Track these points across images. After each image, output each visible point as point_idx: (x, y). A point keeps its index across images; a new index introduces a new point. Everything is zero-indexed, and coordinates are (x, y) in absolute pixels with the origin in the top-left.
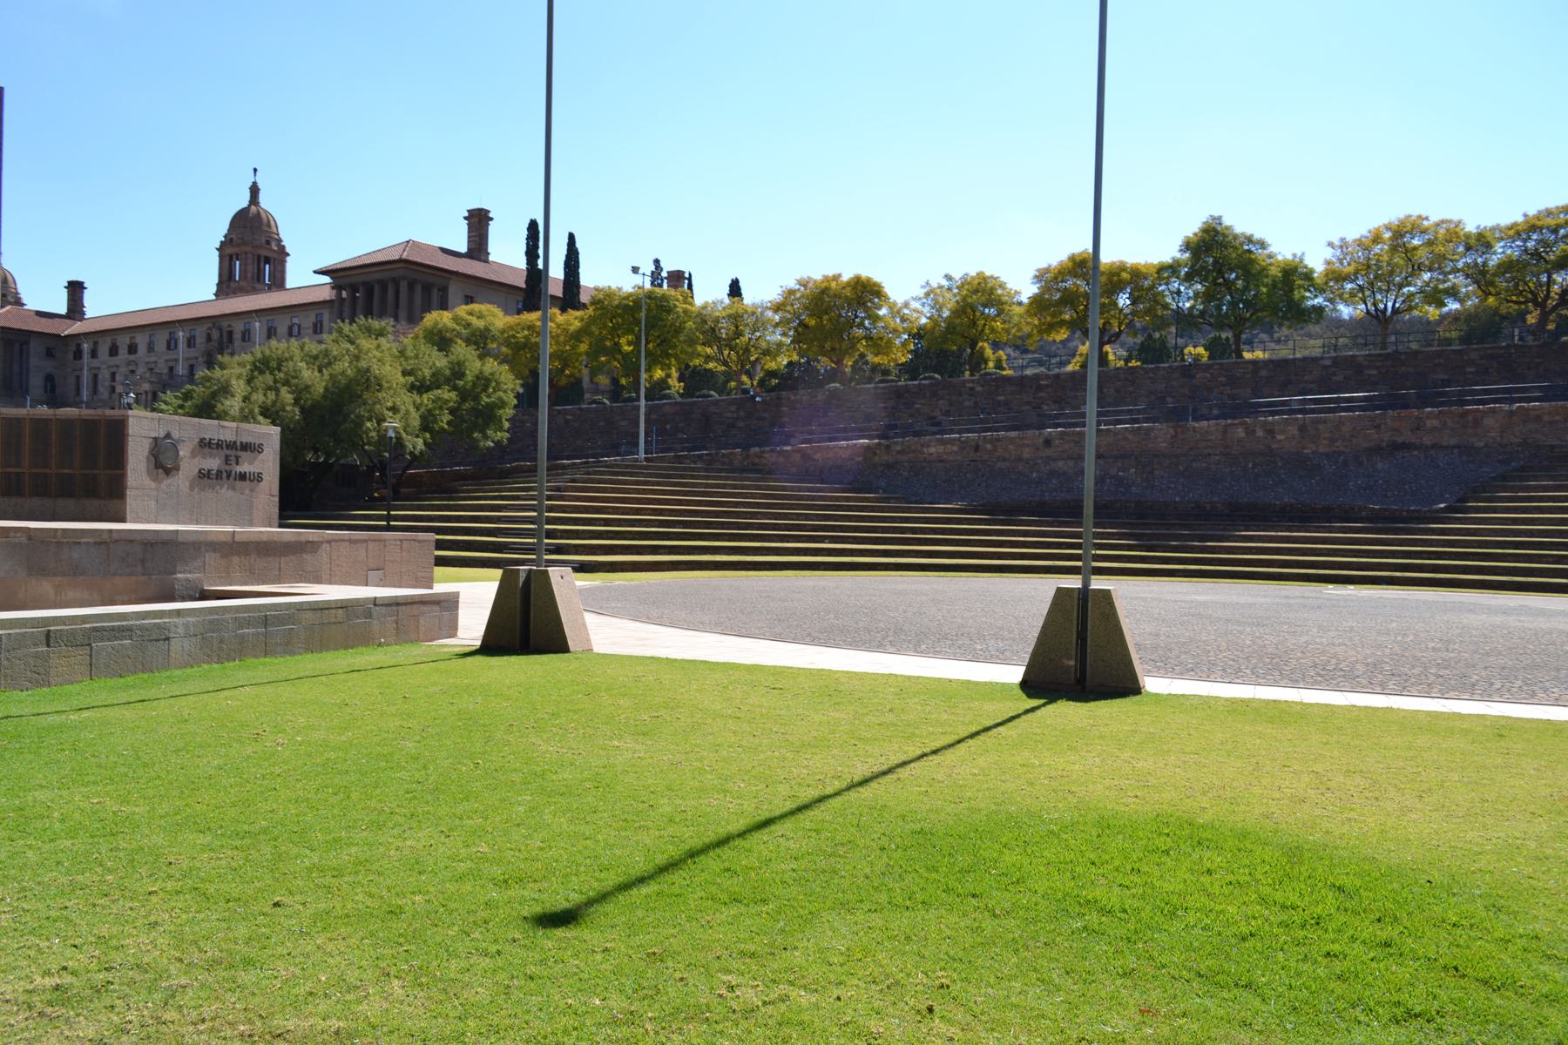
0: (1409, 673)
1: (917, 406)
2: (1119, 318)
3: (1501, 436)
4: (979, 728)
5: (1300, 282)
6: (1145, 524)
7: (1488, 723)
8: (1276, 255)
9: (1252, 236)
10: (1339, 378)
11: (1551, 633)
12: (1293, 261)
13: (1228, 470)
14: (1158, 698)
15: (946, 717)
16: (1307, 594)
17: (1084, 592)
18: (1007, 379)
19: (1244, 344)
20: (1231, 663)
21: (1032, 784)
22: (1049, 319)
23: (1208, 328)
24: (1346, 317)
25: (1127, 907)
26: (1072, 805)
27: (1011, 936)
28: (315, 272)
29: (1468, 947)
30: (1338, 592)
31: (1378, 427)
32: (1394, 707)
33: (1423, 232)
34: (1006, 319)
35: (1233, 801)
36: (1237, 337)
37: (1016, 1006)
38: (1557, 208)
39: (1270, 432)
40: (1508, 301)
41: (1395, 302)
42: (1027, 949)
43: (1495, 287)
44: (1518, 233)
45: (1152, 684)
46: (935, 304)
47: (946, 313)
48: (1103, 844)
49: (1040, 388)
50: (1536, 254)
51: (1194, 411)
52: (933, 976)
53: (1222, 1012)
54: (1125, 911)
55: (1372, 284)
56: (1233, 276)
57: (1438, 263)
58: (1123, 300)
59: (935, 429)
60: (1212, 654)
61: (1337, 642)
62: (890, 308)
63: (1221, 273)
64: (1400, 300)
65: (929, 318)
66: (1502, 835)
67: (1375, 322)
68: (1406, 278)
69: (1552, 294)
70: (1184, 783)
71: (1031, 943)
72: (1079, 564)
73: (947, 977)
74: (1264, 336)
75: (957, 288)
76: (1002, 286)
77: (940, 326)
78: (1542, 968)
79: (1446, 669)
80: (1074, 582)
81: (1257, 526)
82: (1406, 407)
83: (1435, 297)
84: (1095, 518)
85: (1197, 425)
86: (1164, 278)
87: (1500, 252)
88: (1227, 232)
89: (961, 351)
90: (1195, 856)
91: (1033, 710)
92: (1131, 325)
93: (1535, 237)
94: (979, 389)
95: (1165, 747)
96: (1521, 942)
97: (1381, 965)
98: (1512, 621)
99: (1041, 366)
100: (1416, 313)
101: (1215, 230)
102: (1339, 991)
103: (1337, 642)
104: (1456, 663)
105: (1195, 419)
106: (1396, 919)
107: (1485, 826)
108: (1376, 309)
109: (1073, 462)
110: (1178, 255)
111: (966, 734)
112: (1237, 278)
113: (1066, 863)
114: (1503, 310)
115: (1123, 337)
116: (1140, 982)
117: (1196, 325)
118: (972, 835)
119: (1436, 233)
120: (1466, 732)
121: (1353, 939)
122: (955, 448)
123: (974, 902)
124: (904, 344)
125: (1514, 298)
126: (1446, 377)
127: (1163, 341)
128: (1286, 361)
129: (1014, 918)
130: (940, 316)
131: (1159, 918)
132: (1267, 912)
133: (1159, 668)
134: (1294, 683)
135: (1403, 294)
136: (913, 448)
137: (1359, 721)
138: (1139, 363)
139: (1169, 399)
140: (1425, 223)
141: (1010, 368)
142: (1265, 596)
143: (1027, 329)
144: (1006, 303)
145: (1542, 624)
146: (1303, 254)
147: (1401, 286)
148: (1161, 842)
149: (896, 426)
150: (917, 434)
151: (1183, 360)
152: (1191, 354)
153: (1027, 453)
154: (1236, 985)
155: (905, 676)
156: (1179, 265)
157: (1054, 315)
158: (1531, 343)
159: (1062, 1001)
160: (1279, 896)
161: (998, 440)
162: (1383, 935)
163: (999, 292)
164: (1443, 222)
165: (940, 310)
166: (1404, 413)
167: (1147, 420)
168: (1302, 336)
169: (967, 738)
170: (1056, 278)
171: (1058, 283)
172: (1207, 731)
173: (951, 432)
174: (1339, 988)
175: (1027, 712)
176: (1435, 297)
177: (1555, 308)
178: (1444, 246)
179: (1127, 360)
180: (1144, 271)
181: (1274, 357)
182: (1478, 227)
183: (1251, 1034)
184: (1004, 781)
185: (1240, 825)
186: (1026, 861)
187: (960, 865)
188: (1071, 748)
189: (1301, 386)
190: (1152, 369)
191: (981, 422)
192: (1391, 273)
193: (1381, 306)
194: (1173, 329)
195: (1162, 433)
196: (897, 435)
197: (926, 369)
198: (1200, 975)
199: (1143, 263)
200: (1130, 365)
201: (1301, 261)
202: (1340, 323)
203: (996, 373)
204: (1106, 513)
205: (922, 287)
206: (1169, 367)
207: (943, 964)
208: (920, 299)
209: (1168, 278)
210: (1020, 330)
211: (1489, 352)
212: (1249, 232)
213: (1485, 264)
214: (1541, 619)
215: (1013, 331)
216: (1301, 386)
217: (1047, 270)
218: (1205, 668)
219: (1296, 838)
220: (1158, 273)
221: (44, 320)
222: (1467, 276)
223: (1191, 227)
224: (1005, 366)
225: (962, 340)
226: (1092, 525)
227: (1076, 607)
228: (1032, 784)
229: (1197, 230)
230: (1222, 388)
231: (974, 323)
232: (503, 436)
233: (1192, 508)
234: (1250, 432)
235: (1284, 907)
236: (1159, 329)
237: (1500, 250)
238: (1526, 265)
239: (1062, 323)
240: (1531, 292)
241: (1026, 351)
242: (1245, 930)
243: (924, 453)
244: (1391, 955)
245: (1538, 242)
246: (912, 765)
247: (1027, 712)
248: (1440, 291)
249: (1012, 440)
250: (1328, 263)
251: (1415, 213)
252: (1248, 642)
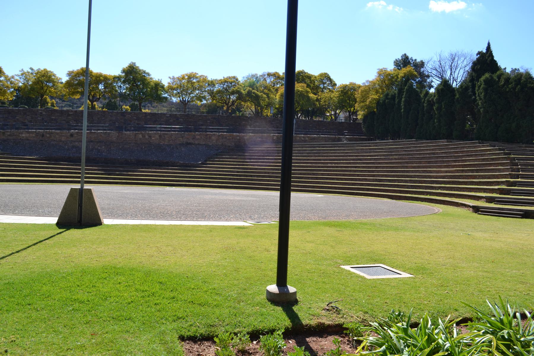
0: (188, 214)
2: (99, 93)
3: (216, 142)
4: (38, 241)
5: (160, 88)
6: (108, 166)
7: (208, 227)
8: (153, 78)
9: (145, 71)
10: (171, 121)
11: (227, 200)
12: (158, 81)
13: (136, 148)
14: (108, 226)
15: (24, 238)
16: (160, 190)
17: (81, 190)
18: (56, 110)
19: (142, 107)
20: (134, 213)
21: (57, 260)
22: (73, 90)
23: (131, 100)
24: (175, 102)
25: (89, 299)
26: (73, 266)
27: (43, 317)
29: (196, 295)
30: (170, 189)
31: (183, 137)
32: (183, 224)
33: (197, 78)
34: (56, 88)
35: (130, 259)
36: (140, 104)
37: (43, 342)
38: (232, 77)
39: (150, 137)
40: (219, 102)
41: (188, 99)
42: (49, 320)
43: (216, 98)
44: (222, 82)
45: (106, 221)
46: (26, 79)
47: (30, 83)
48: (83, 279)
49: (69, 115)
50: (226, 89)
51: (125, 128)
52: (9, 338)
53: (120, 329)
54: (89, 301)
55: (182, 92)
56: (139, 83)
57: (200, 88)
58: (101, 87)
59: (25, 127)
60: (128, 210)
61: (168, 205)
62: (5, 77)
63: (135, 82)
64: (190, 98)
65: (23, 84)
66: (208, 260)
67: (182, 104)
68: (192, 92)
69: (230, 102)
70: (114, 254)
71: (52, 318)
72: (85, 180)
73: (14, 338)
74: (149, 105)
75: (35, 73)
76: (54, 75)
77: (28, 87)
78: (215, 297)
79: (198, 212)
80: (78, 186)
81: (146, 167)
82: (191, 131)
83: (200, 98)
84: (86, 163)
85: (126, 133)
86: (115, 81)
87: (217, 88)
88: (137, 68)
89: (37, 98)
90: (115, 279)
91: (60, 233)
92: (104, 96)
93: (226, 84)
94: (44, 113)
95: (109, 243)
96: (210, 291)
97: (171, 304)
98: (217, 197)
99: (70, 107)
100: (194, 103)
101: (133, 67)
102: (158, 315)
103: (168, 205)
104: (201, 210)
105: (125, 131)
106: (177, 289)
107: (204, 258)
108: (183, 100)
109: (78, 143)
110: (121, 74)
111: (32, 244)
112: (140, 84)
113: (68, 287)
114: (218, 105)
115: (101, 100)
116: (92, 325)
117: (126, 98)
118: (31, 282)
119: (200, 79)
120: (202, 230)
121: (163, 298)
122: (34, 135)
123: (29, 307)
124: (12, 93)
125: (220, 101)
126: (202, 123)
127: (115, 103)
128: (155, 114)
129: (45, 310)
130: (28, 83)
131: (101, 301)
132: (137, 294)
133: (109, 216)
134: (154, 218)
135: (191, 96)
136: (15, 134)
137: (172, 229)
138: (106, 110)
139: (117, 123)
140: (197, 75)
141: (57, 107)
142: (147, 191)
143: (64, 93)
144: (56, 82)
145: (225, 197)
146: (161, 79)
147: (190, 94)
148: (103, 276)
149: (7, 125)
150: (17, 129)
151: (122, 110)
152: (124, 108)
153: (63, 139)
154: (125, 319)
155: (7, 223)
156: (121, 78)
157: (75, 89)
158: (224, 115)
159: (62, 337)
160: (142, 288)
161: (52, 133)
162: (172, 295)
163: (53, 77)
164: (202, 76)
165: (28, 81)
166: (190, 133)
167: (109, 130)
168: (161, 106)
169: (32, 245)
170: (76, 75)
171: (77, 77)
172: (124, 236)
173: (32, 129)
174: (158, 314)
175: (58, 234)
176: (200, 98)
177: (231, 106)
178: (202, 83)
179: (103, 108)
180: (109, 77)
181: (152, 112)
182: (211, 79)
183: (129, 334)
184: (46, 260)
185: (131, 266)
186: (52, 288)
187: (25, 294)
188: (74, 246)
189: (160, 122)
190: (111, 112)
191: (45, 126)
192: (187, 89)
193: (184, 99)
194: (119, 99)
195: (114, 134)
196: (8, 129)
197: (22, 104)
198: (113, 318)
199: (108, 74)
200: (103, 110)
201: (161, 82)
202: (172, 103)
203: (51, 108)
204: (90, 161)
205: (20, 71)
206: (117, 112)
207: (13, 333)
208: (19, 76)
209: (117, 81)
210: (61, 93)
211: (214, 117)
212: (144, 69)
213: (213, 90)
214: (224, 196)
215: (59, 93)
216: (160, 122)
217: (72, 72)
218: (125, 215)
219: (149, 269)
220: (113, 79)
222: (208, 93)
223: (126, 65)
224: (55, 106)
225: (37, 94)
226: (85, 166)
227: (78, 195)
228: (57, 260)
229: (127, 66)
231: (42, 88)
232: (434, 108)
233: (124, 161)
234: (144, 136)
235: (143, 291)
236: (114, 99)
237: (217, 87)
238: (224, 92)
239: (78, 92)
240: (225, 100)
241: (64, 101)
242: (130, 301)
243: (20, 136)
244: (174, 301)
245: (227, 86)
246: (7, 258)
247: (58, 234)
248: (201, 97)
249: (57, 134)
250: (169, 83)
251: (194, 72)
252: (140, 206)
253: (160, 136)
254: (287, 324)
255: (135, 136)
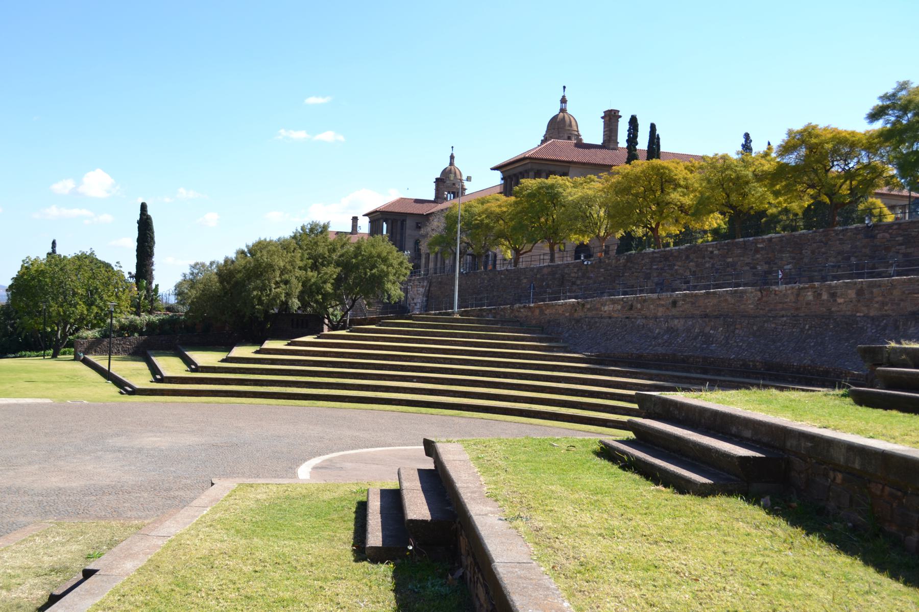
1: (676, 267)
28: (492, 169)
39: (833, 295)
49: (757, 251)
94: (716, 252)
161: (645, 301)
221: (418, 205)
230: (897, 247)
249: (653, 300)
253: (860, 293)
254: (423, 512)
255: (798, 295)
